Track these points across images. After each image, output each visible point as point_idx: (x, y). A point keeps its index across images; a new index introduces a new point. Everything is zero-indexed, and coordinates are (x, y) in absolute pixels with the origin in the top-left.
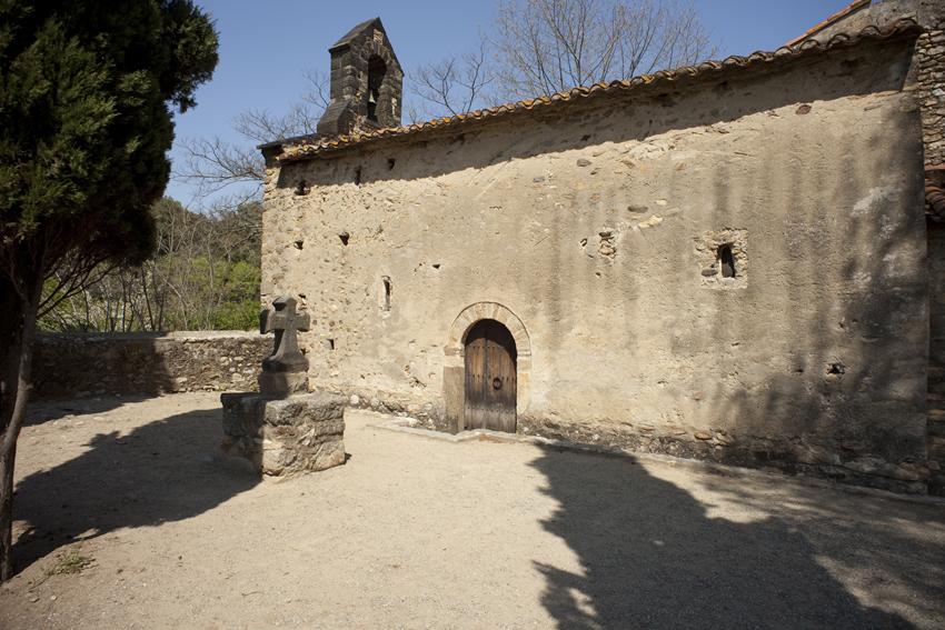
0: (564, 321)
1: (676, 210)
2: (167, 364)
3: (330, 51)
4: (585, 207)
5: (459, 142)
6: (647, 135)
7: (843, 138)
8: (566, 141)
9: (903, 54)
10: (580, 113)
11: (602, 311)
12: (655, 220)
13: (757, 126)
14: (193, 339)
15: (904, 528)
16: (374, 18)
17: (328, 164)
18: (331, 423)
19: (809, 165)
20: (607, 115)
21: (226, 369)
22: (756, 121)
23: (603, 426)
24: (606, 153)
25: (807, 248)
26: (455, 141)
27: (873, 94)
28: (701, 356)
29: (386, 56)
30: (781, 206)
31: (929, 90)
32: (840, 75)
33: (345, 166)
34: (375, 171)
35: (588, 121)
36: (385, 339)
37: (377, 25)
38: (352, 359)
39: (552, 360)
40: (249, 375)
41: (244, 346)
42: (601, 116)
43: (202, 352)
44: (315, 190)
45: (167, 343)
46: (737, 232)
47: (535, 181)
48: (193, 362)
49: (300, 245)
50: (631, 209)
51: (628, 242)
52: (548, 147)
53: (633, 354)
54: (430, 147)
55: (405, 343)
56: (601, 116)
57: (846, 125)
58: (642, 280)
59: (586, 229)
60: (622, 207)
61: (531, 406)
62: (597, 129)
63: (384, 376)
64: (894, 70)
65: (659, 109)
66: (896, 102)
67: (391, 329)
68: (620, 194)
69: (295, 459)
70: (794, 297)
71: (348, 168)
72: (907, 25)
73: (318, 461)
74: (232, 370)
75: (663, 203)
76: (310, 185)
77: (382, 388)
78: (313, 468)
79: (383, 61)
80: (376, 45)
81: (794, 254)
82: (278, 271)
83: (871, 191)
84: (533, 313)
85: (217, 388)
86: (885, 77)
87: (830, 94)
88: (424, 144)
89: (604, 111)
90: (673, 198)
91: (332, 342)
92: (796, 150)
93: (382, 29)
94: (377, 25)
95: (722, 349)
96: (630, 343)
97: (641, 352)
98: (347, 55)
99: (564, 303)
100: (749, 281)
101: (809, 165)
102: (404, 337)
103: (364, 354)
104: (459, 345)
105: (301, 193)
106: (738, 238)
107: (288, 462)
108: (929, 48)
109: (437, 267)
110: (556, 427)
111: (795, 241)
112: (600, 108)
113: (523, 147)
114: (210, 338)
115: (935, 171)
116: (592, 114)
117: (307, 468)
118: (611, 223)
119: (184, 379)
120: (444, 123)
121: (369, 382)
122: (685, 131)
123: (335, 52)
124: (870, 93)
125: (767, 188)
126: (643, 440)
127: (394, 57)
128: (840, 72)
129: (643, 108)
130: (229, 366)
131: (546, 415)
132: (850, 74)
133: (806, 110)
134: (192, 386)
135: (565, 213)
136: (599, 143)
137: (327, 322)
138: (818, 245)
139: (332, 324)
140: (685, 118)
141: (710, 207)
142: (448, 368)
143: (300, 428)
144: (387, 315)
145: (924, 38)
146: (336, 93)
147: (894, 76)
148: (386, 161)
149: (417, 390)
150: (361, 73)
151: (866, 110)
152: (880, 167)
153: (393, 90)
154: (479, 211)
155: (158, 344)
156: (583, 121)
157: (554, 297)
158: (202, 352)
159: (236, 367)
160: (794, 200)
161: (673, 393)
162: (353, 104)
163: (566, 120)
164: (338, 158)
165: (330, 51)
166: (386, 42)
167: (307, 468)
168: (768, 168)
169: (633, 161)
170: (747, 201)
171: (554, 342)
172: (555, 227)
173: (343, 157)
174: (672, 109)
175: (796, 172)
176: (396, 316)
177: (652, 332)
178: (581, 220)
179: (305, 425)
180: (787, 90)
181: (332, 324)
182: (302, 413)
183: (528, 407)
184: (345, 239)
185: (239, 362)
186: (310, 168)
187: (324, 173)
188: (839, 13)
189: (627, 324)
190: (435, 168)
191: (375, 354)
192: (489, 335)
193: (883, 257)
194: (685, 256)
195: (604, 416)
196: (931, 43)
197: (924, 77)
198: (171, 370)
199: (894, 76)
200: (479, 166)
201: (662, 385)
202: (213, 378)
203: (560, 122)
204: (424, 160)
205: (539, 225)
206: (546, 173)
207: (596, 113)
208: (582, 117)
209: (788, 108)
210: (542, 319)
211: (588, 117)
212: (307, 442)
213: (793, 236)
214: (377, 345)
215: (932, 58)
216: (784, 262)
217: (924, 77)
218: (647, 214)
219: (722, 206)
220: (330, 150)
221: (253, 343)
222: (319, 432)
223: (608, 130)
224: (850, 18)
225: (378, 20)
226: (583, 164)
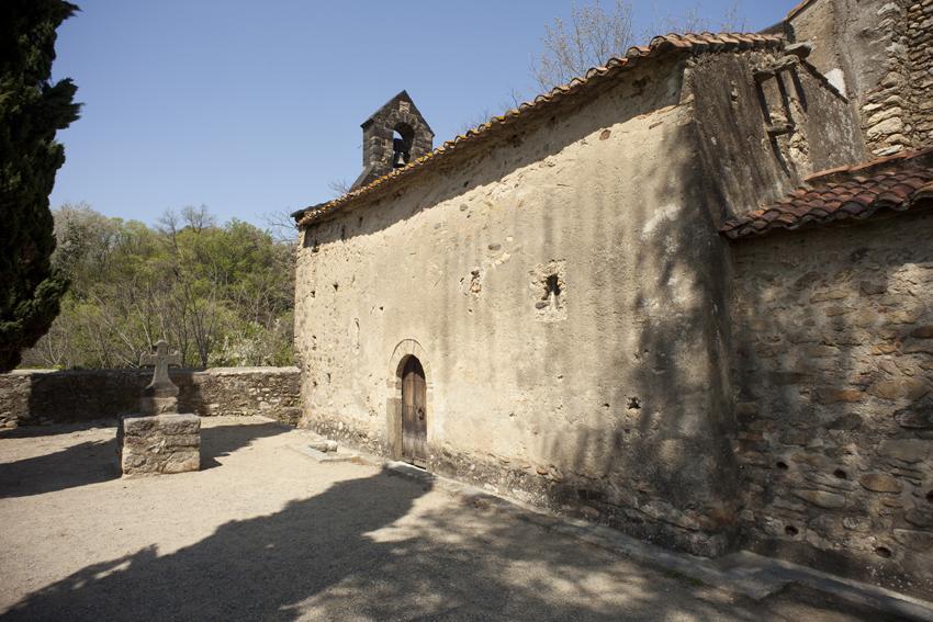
0: (451, 356)
1: (519, 245)
2: (202, 393)
4: (463, 249)
6: (502, 176)
7: (634, 159)
9: (676, 67)
11: (474, 346)
12: (506, 256)
13: (574, 156)
14: (225, 373)
15: (633, 571)
16: (401, 91)
18: (184, 437)
19: (609, 190)
21: (254, 398)
22: (573, 150)
23: (478, 456)
24: (477, 196)
25: (608, 277)
27: (657, 111)
28: (538, 389)
29: (413, 123)
30: (588, 238)
31: (924, 69)
32: (632, 97)
37: (404, 96)
40: (275, 403)
41: (271, 379)
43: (233, 384)
44: (322, 248)
45: (202, 377)
46: (559, 263)
47: (436, 228)
48: (225, 392)
50: (491, 248)
51: (488, 279)
52: (445, 195)
53: (493, 386)
54: (382, 204)
55: (366, 377)
57: (637, 145)
58: (497, 315)
59: (464, 269)
60: (485, 246)
62: (474, 175)
64: (671, 83)
65: (511, 150)
66: (675, 117)
67: (359, 365)
68: (483, 234)
69: (144, 462)
70: (601, 328)
72: (660, 42)
73: (168, 465)
74: (260, 399)
75: (510, 239)
78: (162, 471)
79: (410, 127)
80: (402, 115)
81: (598, 282)
82: (303, 317)
83: (656, 211)
84: (433, 348)
86: (664, 93)
87: (625, 117)
89: (478, 157)
90: (518, 235)
91: (329, 375)
92: (599, 176)
93: (409, 101)
94: (404, 96)
95: (550, 382)
96: (491, 377)
97: (498, 386)
98: (372, 128)
100: (568, 312)
101: (609, 190)
103: (346, 387)
104: (395, 379)
105: (315, 251)
106: (560, 269)
107: (136, 464)
108: (921, 21)
109: (382, 308)
110: (448, 455)
111: (600, 269)
112: (473, 156)
113: (431, 198)
114: (240, 373)
115: (837, 173)
117: (157, 470)
118: (478, 262)
119: (217, 405)
122: (525, 168)
123: (365, 126)
124: (654, 110)
125: (579, 217)
126: (502, 472)
127: (423, 121)
128: (632, 93)
129: (502, 150)
130: (257, 396)
131: (444, 445)
132: (639, 94)
133: (606, 135)
134: (222, 411)
136: (473, 188)
137: (326, 358)
138: (616, 268)
139: (329, 361)
140: (527, 156)
141: (541, 240)
143: (150, 439)
144: (357, 352)
145: (915, 10)
146: (366, 162)
147: (672, 90)
150: (386, 141)
151: (650, 128)
152: (664, 194)
153: (422, 150)
155: (195, 377)
157: (443, 331)
158: (233, 384)
159: (264, 396)
160: (598, 226)
161: (519, 425)
162: (378, 168)
166: (413, 110)
167: (157, 470)
168: (579, 197)
169: (492, 202)
170: (566, 231)
171: (446, 377)
174: (519, 149)
175: (598, 196)
176: (362, 353)
177: (504, 366)
179: (155, 438)
180: (594, 118)
181: (329, 361)
182: (153, 429)
185: (266, 393)
186: (320, 228)
188: (799, 6)
189: (489, 358)
190: (383, 222)
191: (351, 387)
192: (411, 368)
194: (524, 290)
196: (924, 14)
197: (917, 55)
198: (206, 397)
199: (672, 90)
200: (406, 218)
201: (513, 418)
202: (243, 405)
206: (443, 219)
209: (593, 134)
210: (439, 354)
211: (469, 164)
212: (157, 451)
213: (597, 264)
215: (926, 32)
216: (592, 292)
217: (917, 55)
218: (500, 252)
219: (549, 240)
221: (278, 377)
222: (169, 443)
223: (480, 175)
224: (810, 8)
225: (404, 93)
226: (463, 208)
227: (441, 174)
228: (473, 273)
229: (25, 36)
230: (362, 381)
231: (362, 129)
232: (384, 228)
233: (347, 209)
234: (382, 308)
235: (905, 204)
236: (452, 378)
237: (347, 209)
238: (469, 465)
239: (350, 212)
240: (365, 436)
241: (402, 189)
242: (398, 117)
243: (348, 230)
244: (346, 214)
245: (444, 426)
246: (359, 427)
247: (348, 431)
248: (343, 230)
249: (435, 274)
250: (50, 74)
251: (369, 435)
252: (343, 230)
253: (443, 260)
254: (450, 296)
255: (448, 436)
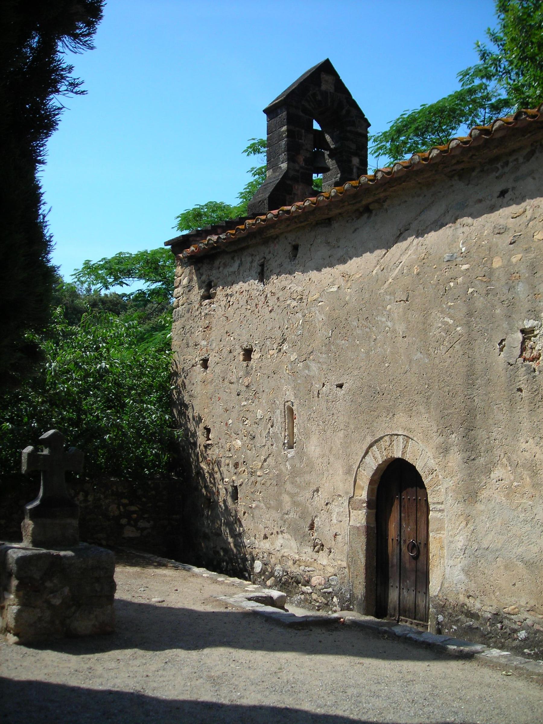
3: (265, 111)
5: (366, 215)
8: (480, 201)
10: (497, 159)
16: (326, 58)
17: (233, 258)
20: (528, 158)
26: (361, 214)
33: (249, 259)
34: (278, 262)
35: (506, 169)
36: (289, 486)
38: (256, 512)
39: (468, 519)
42: (521, 160)
49: (205, 363)
54: (335, 225)
56: (521, 160)
61: (446, 585)
62: (516, 180)
63: (286, 536)
71: (252, 262)
74: (124, 521)
76: (216, 286)
77: (286, 552)
85: (104, 543)
88: (328, 222)
89: (525, 152)
99: (481, 434)
102: (308, 484)
109: (340, 386)
112: (513, 152)
113: (431, 215)
116: (511, 159)
120: (48, 253)
121: (272, 544)
131: (462, 598)
135: (480, 303)
139: (236, 465)
142: (353, 527)
144: (291, 453)
148: (289, 249)
149: (323, 559)
154: (384, 308)
156: (499, 172)
163: (482, 171)
164: (243, 249)
165: (265, 111)
172: (468, 324)
173: (247, 247)
176: (301, 454)
178: (498, 311)
181: (236, 465)
183: (442, 584)
184: (248, 353)
186: (217, 263)
187: (226, 272)
190: (340, 253)
191: (279, 505)
193: (281, 597)
195: (532, 603)
203: (474, 174)
204: (328, 243)
205: (451, 322)
207: (514, 157)
208: (499, 165)
211: (507, 163)
214: (281, 494)
220: (230, 243)
223: (530, 180)
226: (500, 232)
227: (451, 177)
228: (523, 331)
229: (34, 45)
230: (299, 499)
231: (265, 116)
232: (344, 262)
233: (272, 232)
234: (340, 386)
235: (471, 106)
236: (484, 494)
237: (272, 232)
238: (515, 631)
239: (275, 238)
240: (307, 583)
241: (378, 201)
242: (319, 98)
243: (273, 264)
244: (266, 241)
245: (467, 571)
246: (295, 570)
247: (272, 574)
248: (262, 265)
249: (447, 331)
250: (366, 120)
251: (315, 581)
252: (262, 265)
253: (465, 310)
254: (479, 367)
255: (473, 585)
